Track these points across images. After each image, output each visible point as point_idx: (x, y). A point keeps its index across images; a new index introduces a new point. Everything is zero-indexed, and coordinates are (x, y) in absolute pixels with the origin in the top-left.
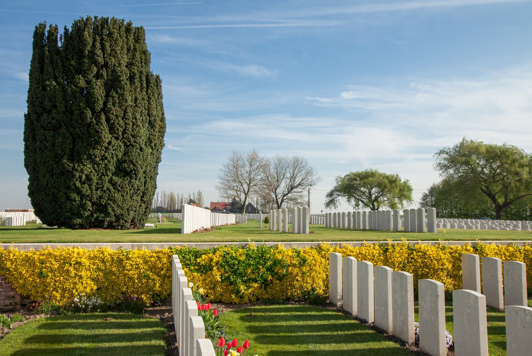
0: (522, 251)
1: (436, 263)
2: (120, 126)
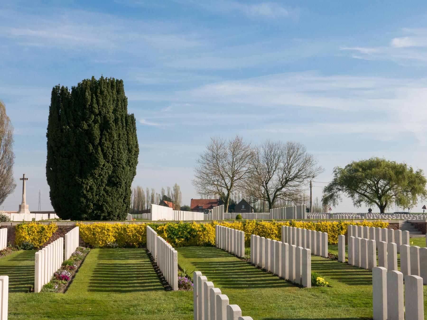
0: (315, 225)
1: (269, 230)
2: (110, 154)
